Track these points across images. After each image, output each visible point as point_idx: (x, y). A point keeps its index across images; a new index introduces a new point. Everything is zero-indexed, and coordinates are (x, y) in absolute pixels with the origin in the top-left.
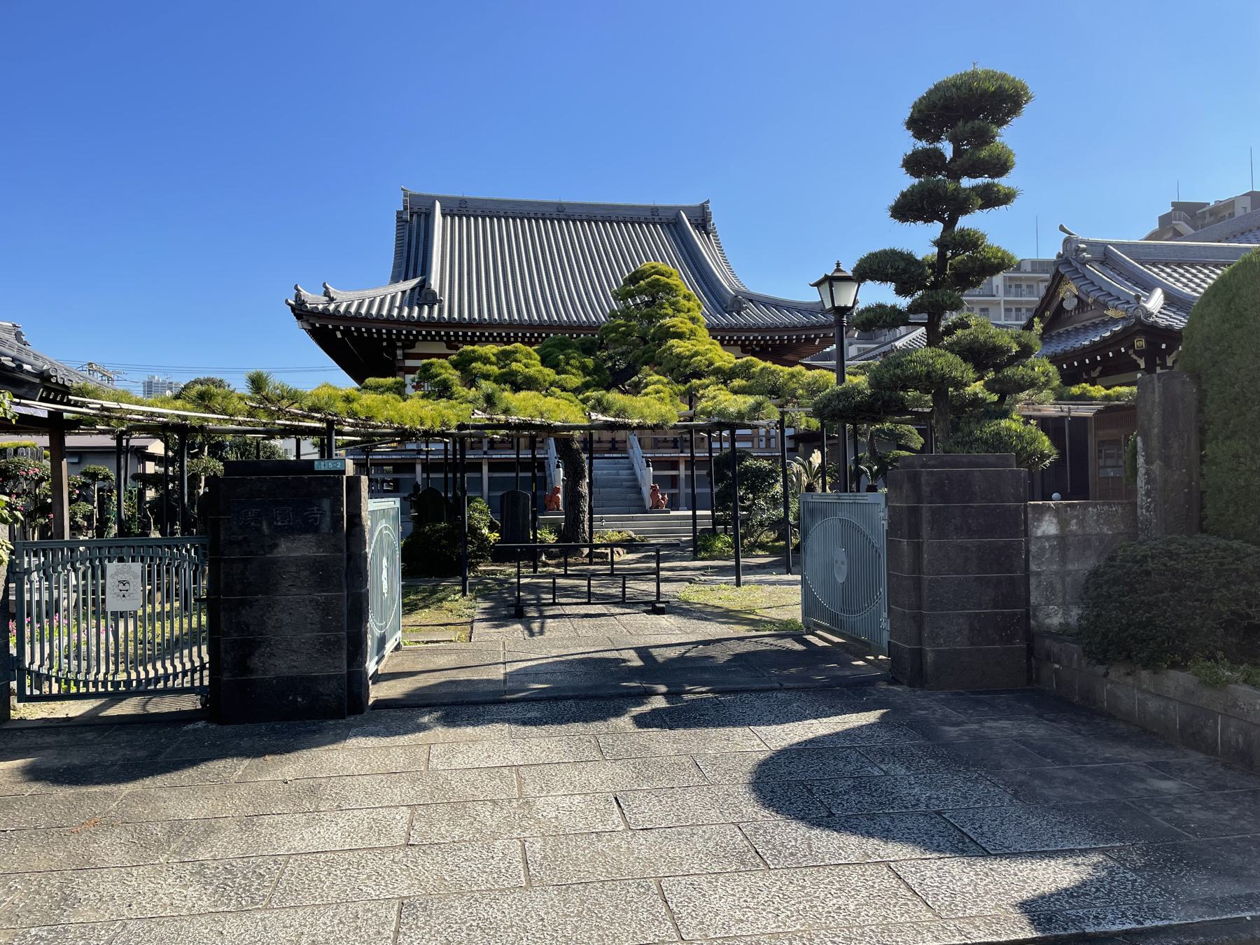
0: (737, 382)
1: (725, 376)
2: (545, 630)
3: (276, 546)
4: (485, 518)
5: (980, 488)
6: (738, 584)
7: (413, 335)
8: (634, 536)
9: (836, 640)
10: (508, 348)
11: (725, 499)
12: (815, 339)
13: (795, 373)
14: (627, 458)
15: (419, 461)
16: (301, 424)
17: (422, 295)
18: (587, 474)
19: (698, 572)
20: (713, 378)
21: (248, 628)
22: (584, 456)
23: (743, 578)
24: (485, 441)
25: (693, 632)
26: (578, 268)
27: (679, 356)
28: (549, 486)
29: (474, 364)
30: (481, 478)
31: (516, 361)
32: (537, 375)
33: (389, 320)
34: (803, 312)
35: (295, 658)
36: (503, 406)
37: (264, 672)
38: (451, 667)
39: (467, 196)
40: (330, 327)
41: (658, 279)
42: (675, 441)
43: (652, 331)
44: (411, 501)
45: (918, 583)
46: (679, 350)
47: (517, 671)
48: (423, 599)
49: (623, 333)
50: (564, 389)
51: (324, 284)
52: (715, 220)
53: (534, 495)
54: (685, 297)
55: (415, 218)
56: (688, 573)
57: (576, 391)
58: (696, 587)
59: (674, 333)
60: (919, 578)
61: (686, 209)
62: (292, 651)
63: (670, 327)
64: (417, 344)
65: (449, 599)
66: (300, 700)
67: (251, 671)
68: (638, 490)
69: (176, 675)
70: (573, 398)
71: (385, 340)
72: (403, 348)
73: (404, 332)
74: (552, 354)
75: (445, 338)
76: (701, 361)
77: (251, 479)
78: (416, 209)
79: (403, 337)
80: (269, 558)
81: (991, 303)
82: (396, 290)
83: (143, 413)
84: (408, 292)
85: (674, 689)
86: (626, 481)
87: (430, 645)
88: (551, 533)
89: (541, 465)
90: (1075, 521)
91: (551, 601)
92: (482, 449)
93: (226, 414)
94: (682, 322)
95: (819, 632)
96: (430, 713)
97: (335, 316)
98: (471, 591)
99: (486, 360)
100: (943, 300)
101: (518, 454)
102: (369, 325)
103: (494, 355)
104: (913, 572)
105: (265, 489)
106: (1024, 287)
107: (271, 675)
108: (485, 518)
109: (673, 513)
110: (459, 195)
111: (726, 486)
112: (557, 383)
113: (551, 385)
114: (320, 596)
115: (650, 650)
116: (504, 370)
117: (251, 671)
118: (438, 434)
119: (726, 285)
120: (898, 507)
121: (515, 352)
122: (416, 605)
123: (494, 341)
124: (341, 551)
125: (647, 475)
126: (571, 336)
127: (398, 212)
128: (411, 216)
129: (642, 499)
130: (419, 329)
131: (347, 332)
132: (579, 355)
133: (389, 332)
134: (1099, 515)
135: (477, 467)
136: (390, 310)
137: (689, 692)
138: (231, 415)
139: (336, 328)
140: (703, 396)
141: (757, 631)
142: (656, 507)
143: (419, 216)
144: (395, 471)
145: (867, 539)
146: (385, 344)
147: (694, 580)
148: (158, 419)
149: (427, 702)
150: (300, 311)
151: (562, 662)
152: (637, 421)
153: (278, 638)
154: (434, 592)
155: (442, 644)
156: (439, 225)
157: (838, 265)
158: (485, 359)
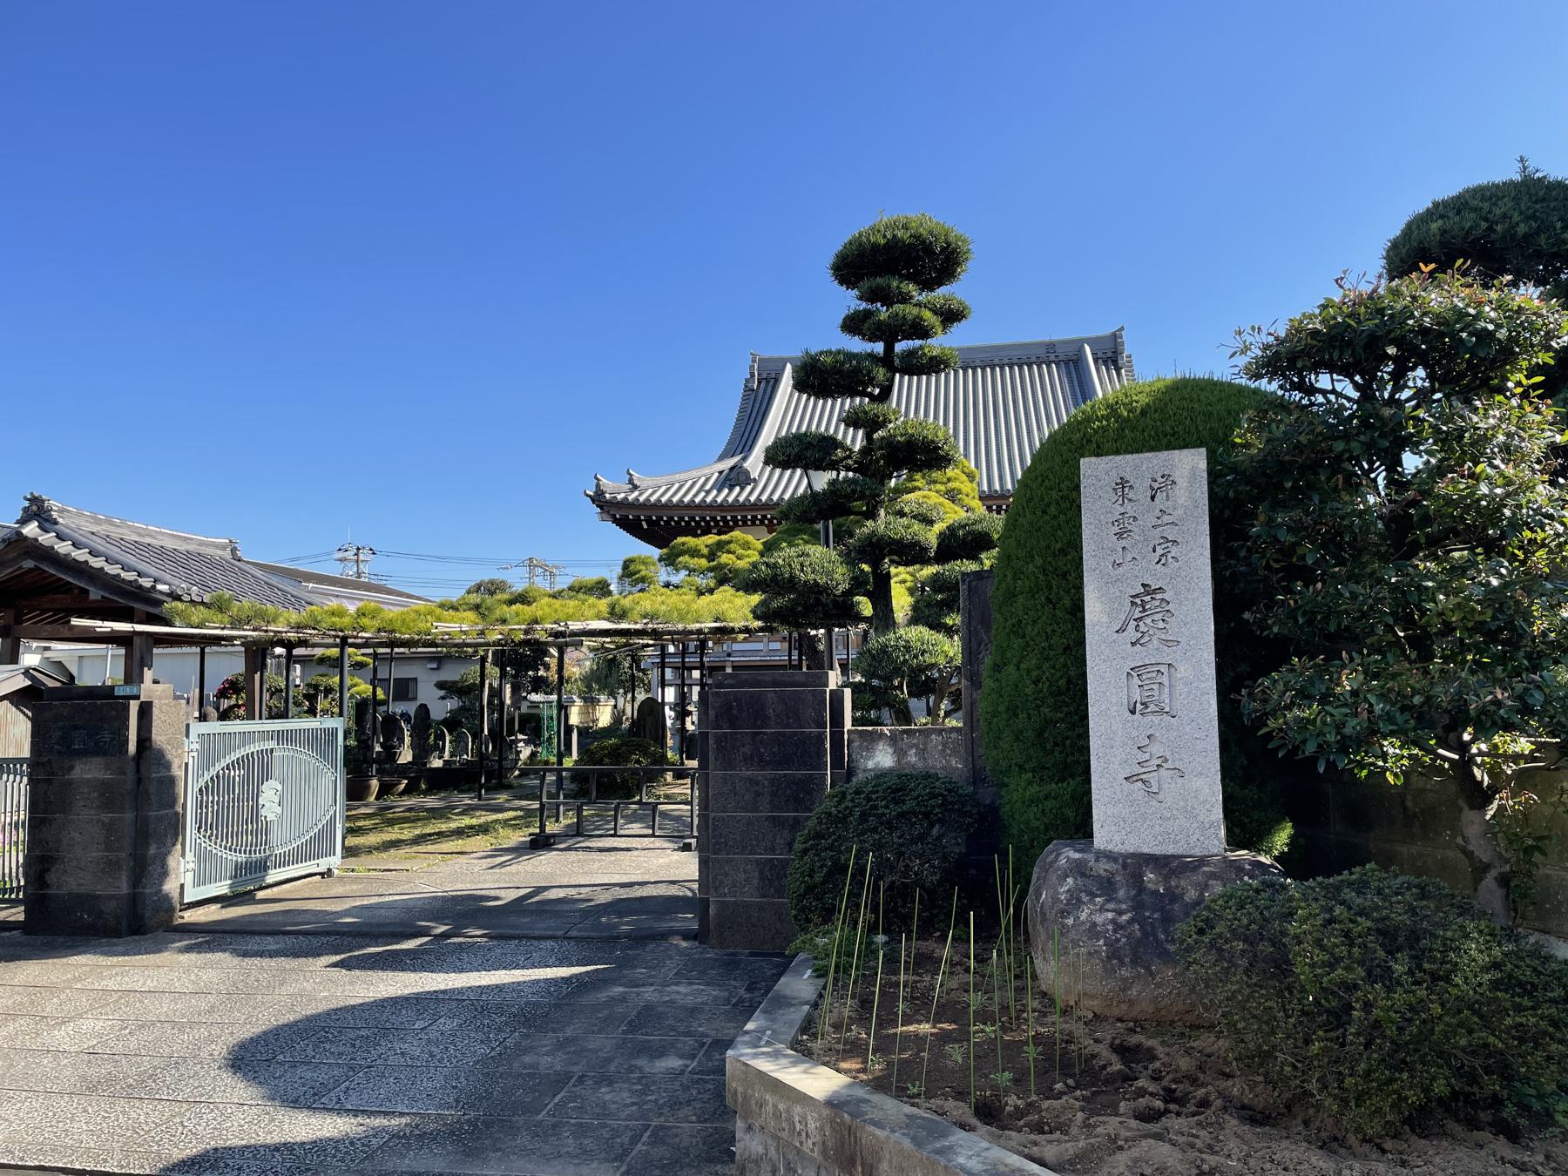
3: (72, 768)
5: (774, 711)
7: (696, 522)
10: (724, 537)
15: (729, 664)
17: (737, 477)
29: (681, 559)
31: (729, 552)
40: (631, 517)
55: (763, 385)
62: (80, 869)
67: (48, 887)
69: (12, 889)
78: (764, 376)
82: (712, 471)
83: (244, 630)
87: (371, 873)
91: (612, 832)
97: (636, 505)
99: (695, 553)
114: (106, 817)
117: (48, 887)
121: (730, 542)
131: (649, 521)
134: (945, 745)
136: (781, 476)
143: (768, 382)
149: (270, 928)
150: (599, 499)
158: (695, 551)
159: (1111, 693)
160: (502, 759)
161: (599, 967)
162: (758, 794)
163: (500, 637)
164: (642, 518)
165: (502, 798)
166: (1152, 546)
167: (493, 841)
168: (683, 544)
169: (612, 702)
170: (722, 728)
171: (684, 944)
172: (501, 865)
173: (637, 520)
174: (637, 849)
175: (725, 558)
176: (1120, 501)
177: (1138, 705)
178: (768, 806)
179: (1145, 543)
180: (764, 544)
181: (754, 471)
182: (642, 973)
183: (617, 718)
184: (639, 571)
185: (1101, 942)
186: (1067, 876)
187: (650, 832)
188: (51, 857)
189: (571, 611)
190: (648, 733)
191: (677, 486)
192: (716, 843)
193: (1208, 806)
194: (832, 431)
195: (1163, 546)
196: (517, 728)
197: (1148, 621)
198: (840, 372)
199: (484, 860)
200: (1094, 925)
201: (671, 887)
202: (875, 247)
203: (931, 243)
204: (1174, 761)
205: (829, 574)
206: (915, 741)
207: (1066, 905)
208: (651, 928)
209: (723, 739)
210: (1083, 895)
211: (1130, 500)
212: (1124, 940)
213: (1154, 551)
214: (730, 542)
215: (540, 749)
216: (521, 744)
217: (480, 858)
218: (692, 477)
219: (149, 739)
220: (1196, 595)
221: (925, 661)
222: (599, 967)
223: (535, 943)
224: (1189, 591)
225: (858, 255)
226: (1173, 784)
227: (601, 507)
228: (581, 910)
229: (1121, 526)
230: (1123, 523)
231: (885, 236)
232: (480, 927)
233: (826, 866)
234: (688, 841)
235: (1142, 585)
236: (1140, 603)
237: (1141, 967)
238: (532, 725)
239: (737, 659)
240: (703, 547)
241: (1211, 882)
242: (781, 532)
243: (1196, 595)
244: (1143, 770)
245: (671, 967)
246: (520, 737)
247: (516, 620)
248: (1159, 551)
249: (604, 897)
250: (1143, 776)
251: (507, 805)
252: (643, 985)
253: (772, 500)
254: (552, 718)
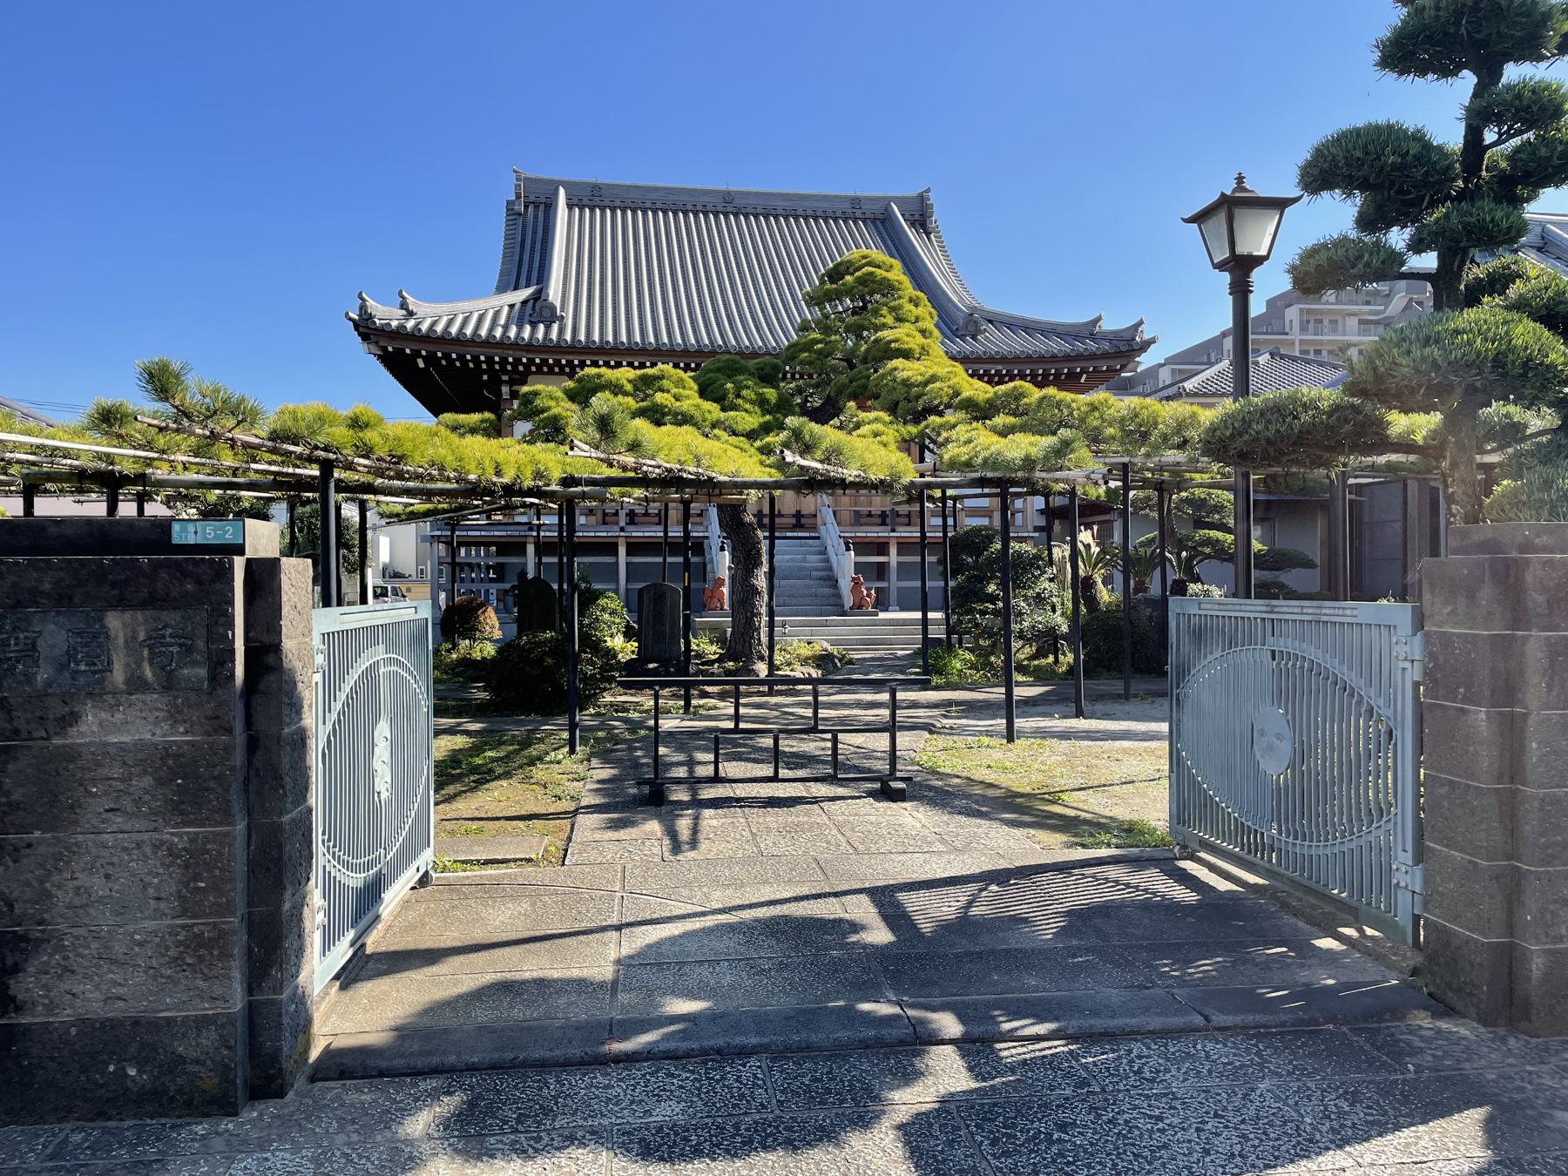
0: (1001, 420)
1: (980, 412)
2: (701, 836)
3: (73, 718)
4: (618, 620)
6: (1010, 736)
7: (523, 364)
8: (830, 648)
9: (1252, 879)
10: (650, 371)
11: (964, 599)
12: (1081, 374)
13: (1097, 404)
14: (818, 538)
16: (298, 471)
17: (537, 310)
18: (765, 558)
19: (936, 712)
20: (961, 415)
21: (11, 907)
22: (760, 534)
23: (1019, 723)
24: (622, 514)
25: (965, 849)
26: (752, 277)
27: (906, 383)
28: (709, 576)
30: (617, 562)
31: (662, 391)
32: (693, 411)
33: (489, 343)
35: (120, 980)
36: (630, 437)
37: (50, 1008)
38: (520, 936)
39: (601, 180)
40: (408, 351)
41: (872, 273)
42: (883, 515)
43: (863, 349)
44: (515, 596)
45: (1510, 807)
46: (905, 374)
47: (641, 954)
48: (508, 758)
49: (820, 352)
50: (734, 433)
51: (401, 292)
52: (938, 217)
53: (687, 590)
54: (911, 300)
55: (530, 209)
56: (921, 712)
57: (751, 435)
58: (941, 741)
59: (897, 350)
60: (1514, 793)
61: (898, 200)
62: (113, 961)
64: (530, 378)
65: (548, 759)
66: (132, 1072)
68: (833, 582)
70: (747, 446)
71: (485, 372)
72: (511, 383)
73: (511, 360)
74: (714, 382)
75: (567, 370)
76: (941, 389)
77: (16, 564)
78: (532, 199)
79: (509, 368)
80: (58, 747)
81: (1283, 342)
84: (518, 306)
85: (977, 1031)
86: (817, 570)
88: (712, 642)
89: (699, 547)
92: (617, 523)
93: (151, 449)
94: (908, 335)
95: (1202, 855)
96: (435, 1095)
97: (415, 337)
98: (584, 741)
99: (616, 389)
100: (1492, 220)
101: (666, 532)
102: (461, 350)
103: (630, 381)
104: (1499, 779)
105: (47, 586)
106: (1326, 322)
107: (66, 1015)
108: (618, 620)
109: (882, 615)
110: (591, 179)
111: (968, 578)
112: (723, 422)
113: (713, 426)
114: (179, 835)
115: (901, 896)
116: (645, 404)
118: (531, 492)
119: (955, 299)
120: (1459, 636)
121: (661, 378)
122: (491, 771)
124: (229, 731)
125: (844, 565)
127: (508, 202)
128: (526, 207)
129: (839, 596)
130: (530, 356)
131: (431, 359)
132: (756, 384)
133: (490, 360)
135: (610, 548)
136: (491, 329)
137: (1010, 1037)
138: (163, 452)
139: (416, 354)
140: (947, 441)
141: (1084, 846)
142: (859, 607)
143: (536, 207)
144: (499, 553)
145: (1359, 703)
146: (485, 377)
147: (934, 726)
148: (64, 462)
150: (366, 328)
151: (731, 928)
152: (855, 473)
153: (81, 931)
154: (526, 743)
155: (512, 870)
156: (563, 219)
157: (1240, 179)
170: (1557, 628)
187: (768, 770)
188: (24, 938)
214: (661, 378)
219: (276, 648)
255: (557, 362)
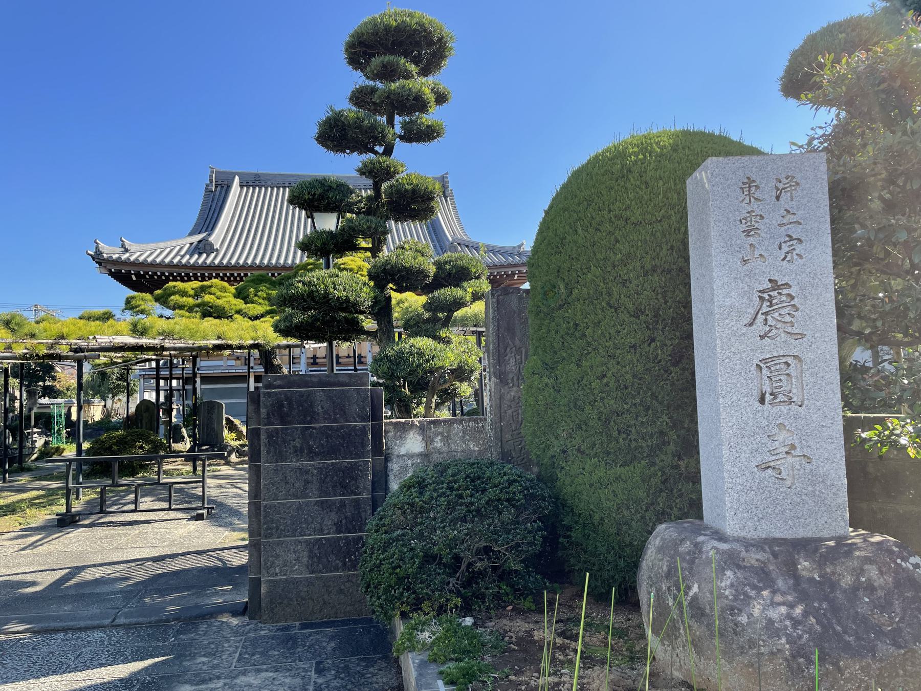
5: (322, 408)
7: (165, 276)
10: (205, 283)
17: (204, 247)
29: (172, 297)
31: (210, 293)
32: (227, 306)
34: (506, 255)
40: (123, 271)
55: (219, 188)
63: (341, 265)
78: (220, 182)
90: (440, 438)
91: (132, 507)
94: (352, 261)
97: (127, 263)
99: (184, 294)
121: (211, 286)
123: (196, 279)
126: (273, 275)
131: (137, 274)
143: (222, 187)
150: (98, 258)
159: (742, 384)
160: (21, 447)
161: (157, 660)
162: (307, 482)
163: (25, 351)
164: (132, 272)
165: (24, 479)
166: (777, 243)
167: (21, 520)
168: (174, 287)
169: (103, 403)
170: (273, 424)
171: (234, 621)
172: (33, 545)
173: (129, 273)
174: (156, 521)
175: (207, 298)
176: (747, 200)
177: (767, 395)
178: (316, 492)
179: (772, 241)
180: (236, 289)
181: (216, 245)
182: (204, 663)
183: (107, 415)
184: (139, 306)
185: (783, 640)
186: (724, 570)
187: (166, 505)
189: (93, 329)
190: (144, 425)
191: (159, 251)
192: (268, 529)
193: (834, 490)
194: (291, 208)
195: (788, 244)
196: (33, 423)
197: (776, 315)
198: (360, 127)
199: (16, 541)
200: (770, 622)
201: (200, 557)
202: (388, 29)
203: (431, 32)
204: (802, 448)
205: (358, 293)
206: (440, 430)
207: (733, 601)
208: (197, 606)
209: (274, 434)
210: (747, 589)
211: (756, 199)
212: (806, 636)
213: (780, 248)
214: (211, 286)
215: (51, 439)
216: (35, 435)
217: (11, 539)
218: (169, 245)
220: (819, 290)
221: (435, 365)
222: (157, 660)
223: (82, 635)
224: (813, 286)
225: (372, 34)
226: (802, 470)
227: (100, 264)
228: (121, 591)
229: (749, 224)
230: (751, 221)
231: (396, 20)
232: (22, 621)
233: (417, 556)
234: (200, 512)
235: (770, 280)
236: (767, 297)
237: (830, 663)
238: (45, 422)
239: (204, 372)
240: (190, 289)
241: (866, 567)
242: (248, 281)
243: (819, 290)
244: (774, 458)
245: (231, 650)
246: (35, 430)
247: (45, 334)
248: (785, 248)
249: (140, 575)
250: (772, 464)
251: (30, 486)
252: (210, 680)
253: (206, 263)
254: (60, 416)
255: (232, 275)
